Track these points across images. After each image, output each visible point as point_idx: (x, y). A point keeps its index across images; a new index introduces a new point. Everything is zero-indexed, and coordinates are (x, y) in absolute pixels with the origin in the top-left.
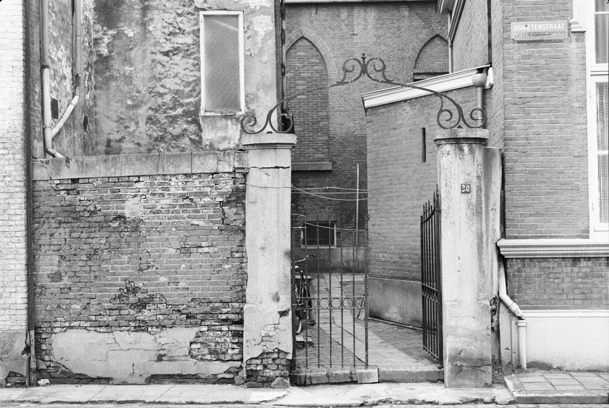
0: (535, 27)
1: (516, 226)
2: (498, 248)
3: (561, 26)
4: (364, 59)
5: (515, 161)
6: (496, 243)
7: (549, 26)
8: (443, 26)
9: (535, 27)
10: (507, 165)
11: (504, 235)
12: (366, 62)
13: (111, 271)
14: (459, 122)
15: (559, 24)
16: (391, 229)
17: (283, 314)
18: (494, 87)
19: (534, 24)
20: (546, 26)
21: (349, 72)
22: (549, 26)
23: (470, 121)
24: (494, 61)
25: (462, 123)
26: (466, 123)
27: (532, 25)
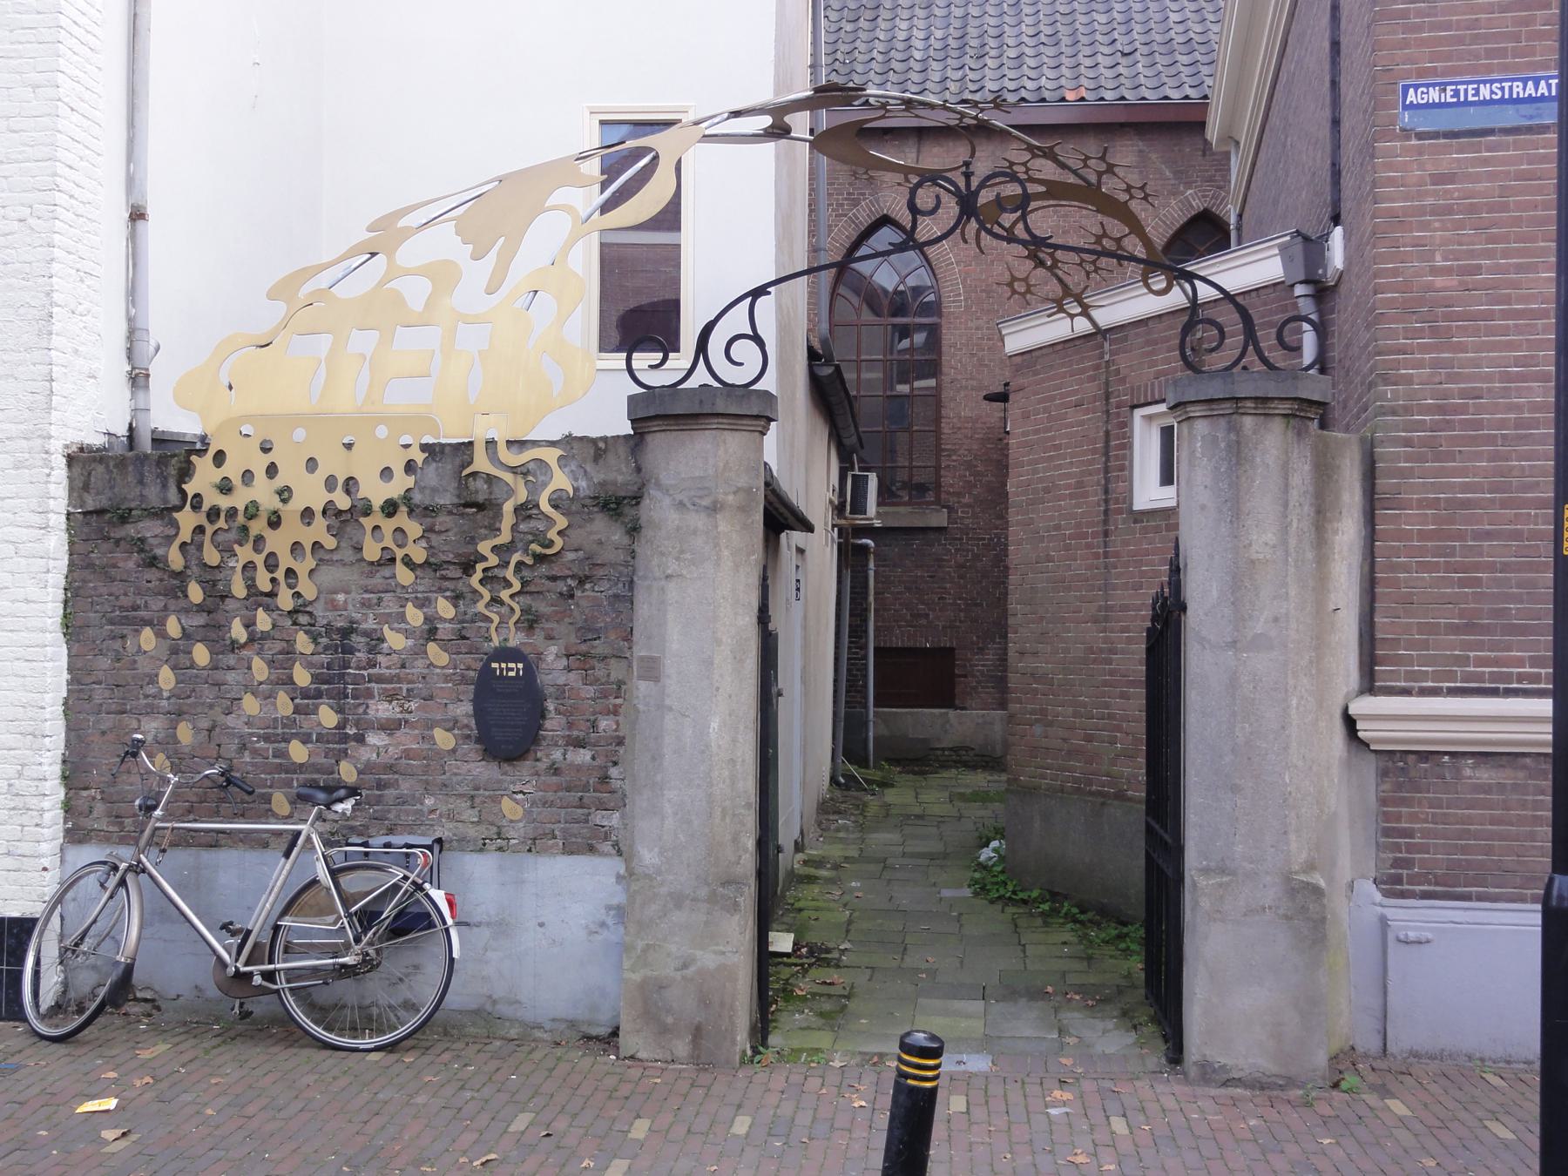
0: (1471, 92)
1: (1399, 660)
2: (1350, 722)
3: (1549, 86)
4: (968, 176)
5: (1402, 473)
6: (1346, 709)
7: (1511, 88)
8: (1220, 188)
9: (1471, 92)
10: (1382, 483)
11: (1369, 686)
12: (975, 183)
13: (272, 760)
14: (1243, 355)
15: (1543, 83)
16: (1064, 640)
17: (350, 485)
18: (1345, 277)
19: (1468, 83)
20: (1502, 89)
21: (924, 214)
22: (1511, 88)
23: (1276, 356)
24: (1346, 206)
25: (1251, 357)
26: (1264, 361)
27: (1462, 88)
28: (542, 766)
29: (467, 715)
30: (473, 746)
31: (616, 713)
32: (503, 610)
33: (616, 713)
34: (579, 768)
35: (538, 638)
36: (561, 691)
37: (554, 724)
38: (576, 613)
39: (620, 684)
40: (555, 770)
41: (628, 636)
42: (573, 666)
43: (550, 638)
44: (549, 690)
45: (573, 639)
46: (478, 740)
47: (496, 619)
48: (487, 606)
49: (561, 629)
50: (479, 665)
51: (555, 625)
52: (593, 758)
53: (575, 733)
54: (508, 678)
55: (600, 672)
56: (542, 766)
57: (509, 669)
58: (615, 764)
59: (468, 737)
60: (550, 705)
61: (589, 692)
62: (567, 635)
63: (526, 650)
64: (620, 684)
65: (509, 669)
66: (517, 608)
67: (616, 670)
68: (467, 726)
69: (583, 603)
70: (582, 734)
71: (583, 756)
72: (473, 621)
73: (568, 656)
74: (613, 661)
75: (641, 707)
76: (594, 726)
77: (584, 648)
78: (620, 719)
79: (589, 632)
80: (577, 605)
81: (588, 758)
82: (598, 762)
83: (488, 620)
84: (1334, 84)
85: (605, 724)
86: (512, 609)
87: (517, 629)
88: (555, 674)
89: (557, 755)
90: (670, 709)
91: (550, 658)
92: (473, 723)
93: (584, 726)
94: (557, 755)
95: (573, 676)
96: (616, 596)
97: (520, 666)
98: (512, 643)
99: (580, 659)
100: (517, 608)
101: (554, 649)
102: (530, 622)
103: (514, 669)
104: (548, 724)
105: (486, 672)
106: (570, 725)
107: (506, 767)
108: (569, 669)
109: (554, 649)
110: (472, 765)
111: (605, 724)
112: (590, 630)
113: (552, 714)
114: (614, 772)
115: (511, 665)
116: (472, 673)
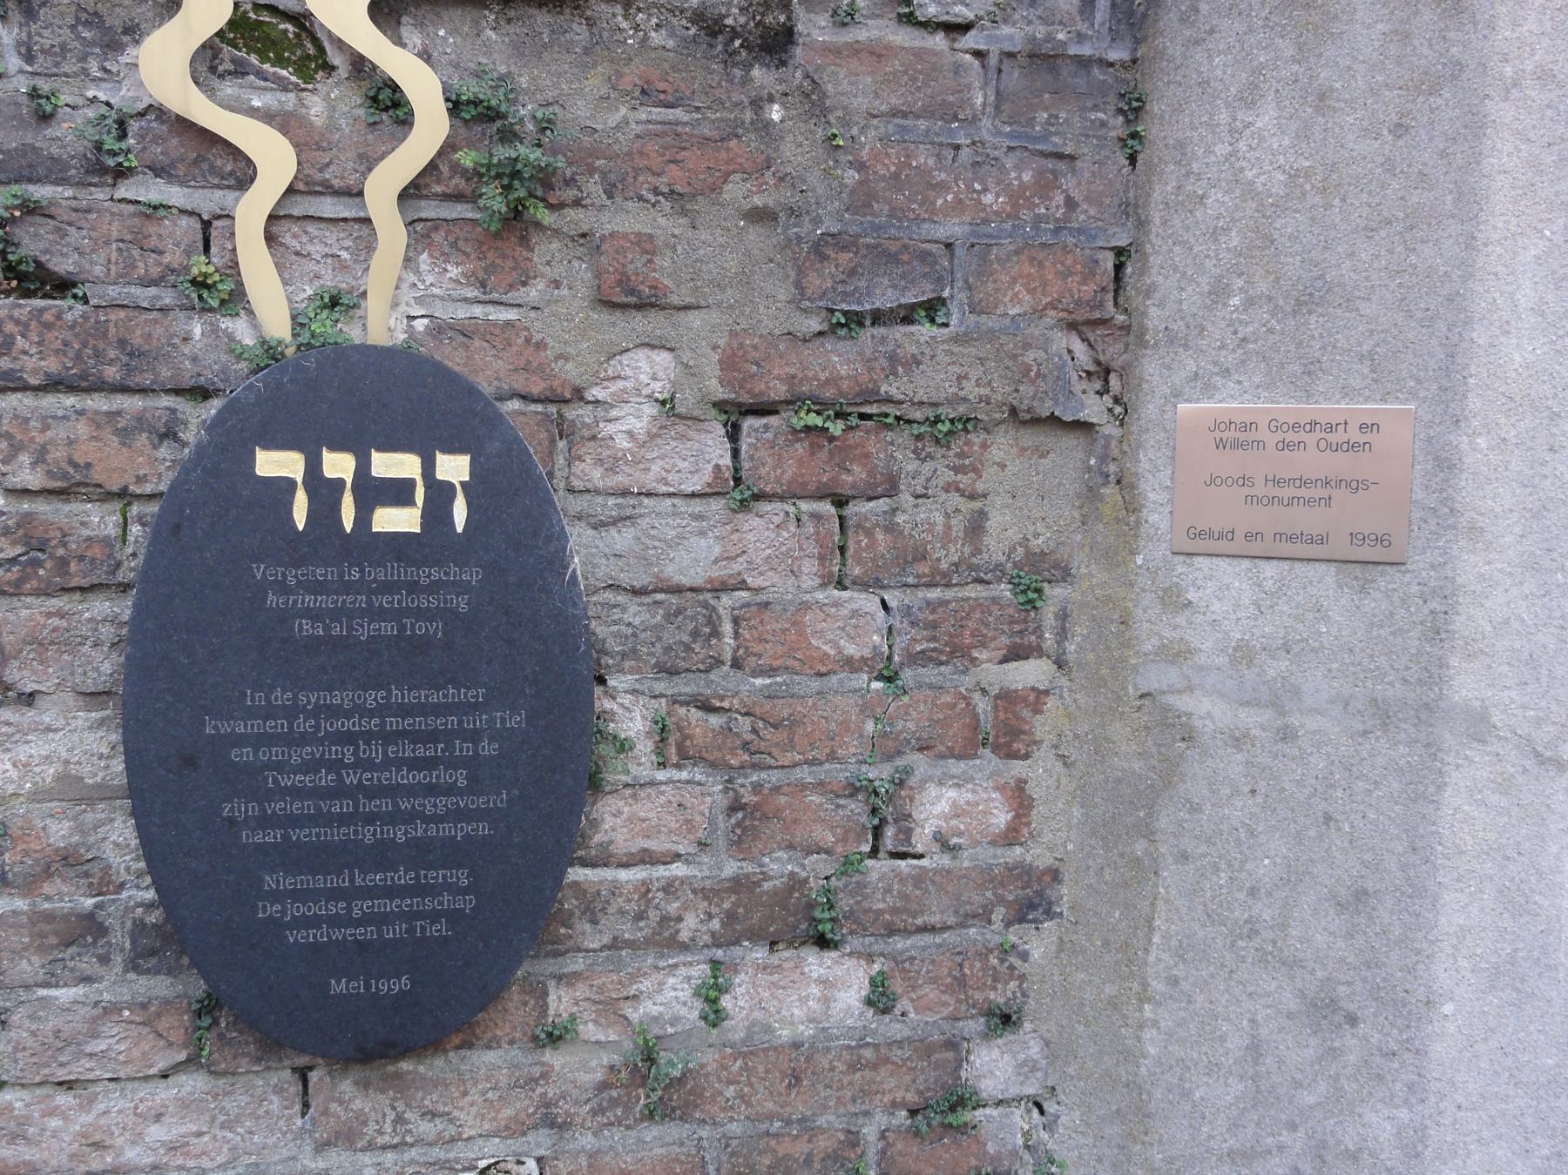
28: (575, 1070)
29: (72, 791)
30: (117, 985)
31: (1009, 739)
32: (328, 104)
33: (1009, 739)
34: (797, 1065)
35: (553, 298)
36: (695, 615)
37: (650, 820)
38: (797, 152)
39: (1034, 575)
40: (651, 1083)
41: (1109, 311)
42: (767, 470)
43: (629, 298)
44: (616, 622)
45: (774, 309)
46: (149, 950)
47: (275, 160)
48: (209, 63)
49: (706, 249)
50: (157, 468)
51: (661, 223)
52: (880, 999)
53: (779, 866)
54: (368, 545)
55: (927, 516)
56: (575, 1070)
57: (374, 492)
58: (1005, 1020)
59: (90, 927)
60: (629, 712)
61: (855, 623)
62: (740, 291)
63: (488, 371)
64: (1034, 575)
65: (374, 492)
66: (424, 89)
67: (1023, 497)
68: (69, 861)
69: (854, 90)
70: (816, 868)
71: (820, 994)
72: (105, 168)
73: (733, 415)
74: (1002, 446)
75: (1207, 710)
76: (884, 819)
77: (841, 363)
78: (1039, 772)
79: (873, 275)
80: (813, 101)
81: (851, 996)
82: (918, 1014)
83: (242, 173)
84: (320, 219)
85: (948, 802)
86: (389, 104)
87: (421, 233)
88: (660, 520)
89: (668, 995)
90: (1478, 725)
91: (629, 423)
92: (117, 839)
93: (830, 821)
94: (668, 995)
95: (762, 531)
96: (1042, 59)
97: (454, 468)
98: (383, 321)
99: (804, 433)
100: (424, 89)
101: (649, 370)
102: (501, 194)
103: (410, 487)
104: (615, 820)
105: (211, 520)
106: (747, 820)
107: (346, 1096)
108: (739, 490)
109: (649, 370)
110: (114, 1105)
111: (948, 802)
112: (886, 257)
113: (642, 763)
114: (993, 1067)
115: (393, 465)
116: (100, 520)
